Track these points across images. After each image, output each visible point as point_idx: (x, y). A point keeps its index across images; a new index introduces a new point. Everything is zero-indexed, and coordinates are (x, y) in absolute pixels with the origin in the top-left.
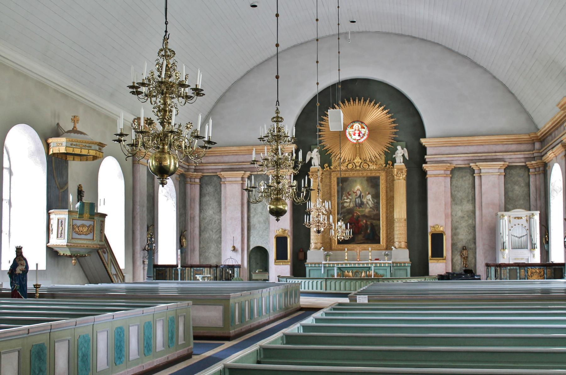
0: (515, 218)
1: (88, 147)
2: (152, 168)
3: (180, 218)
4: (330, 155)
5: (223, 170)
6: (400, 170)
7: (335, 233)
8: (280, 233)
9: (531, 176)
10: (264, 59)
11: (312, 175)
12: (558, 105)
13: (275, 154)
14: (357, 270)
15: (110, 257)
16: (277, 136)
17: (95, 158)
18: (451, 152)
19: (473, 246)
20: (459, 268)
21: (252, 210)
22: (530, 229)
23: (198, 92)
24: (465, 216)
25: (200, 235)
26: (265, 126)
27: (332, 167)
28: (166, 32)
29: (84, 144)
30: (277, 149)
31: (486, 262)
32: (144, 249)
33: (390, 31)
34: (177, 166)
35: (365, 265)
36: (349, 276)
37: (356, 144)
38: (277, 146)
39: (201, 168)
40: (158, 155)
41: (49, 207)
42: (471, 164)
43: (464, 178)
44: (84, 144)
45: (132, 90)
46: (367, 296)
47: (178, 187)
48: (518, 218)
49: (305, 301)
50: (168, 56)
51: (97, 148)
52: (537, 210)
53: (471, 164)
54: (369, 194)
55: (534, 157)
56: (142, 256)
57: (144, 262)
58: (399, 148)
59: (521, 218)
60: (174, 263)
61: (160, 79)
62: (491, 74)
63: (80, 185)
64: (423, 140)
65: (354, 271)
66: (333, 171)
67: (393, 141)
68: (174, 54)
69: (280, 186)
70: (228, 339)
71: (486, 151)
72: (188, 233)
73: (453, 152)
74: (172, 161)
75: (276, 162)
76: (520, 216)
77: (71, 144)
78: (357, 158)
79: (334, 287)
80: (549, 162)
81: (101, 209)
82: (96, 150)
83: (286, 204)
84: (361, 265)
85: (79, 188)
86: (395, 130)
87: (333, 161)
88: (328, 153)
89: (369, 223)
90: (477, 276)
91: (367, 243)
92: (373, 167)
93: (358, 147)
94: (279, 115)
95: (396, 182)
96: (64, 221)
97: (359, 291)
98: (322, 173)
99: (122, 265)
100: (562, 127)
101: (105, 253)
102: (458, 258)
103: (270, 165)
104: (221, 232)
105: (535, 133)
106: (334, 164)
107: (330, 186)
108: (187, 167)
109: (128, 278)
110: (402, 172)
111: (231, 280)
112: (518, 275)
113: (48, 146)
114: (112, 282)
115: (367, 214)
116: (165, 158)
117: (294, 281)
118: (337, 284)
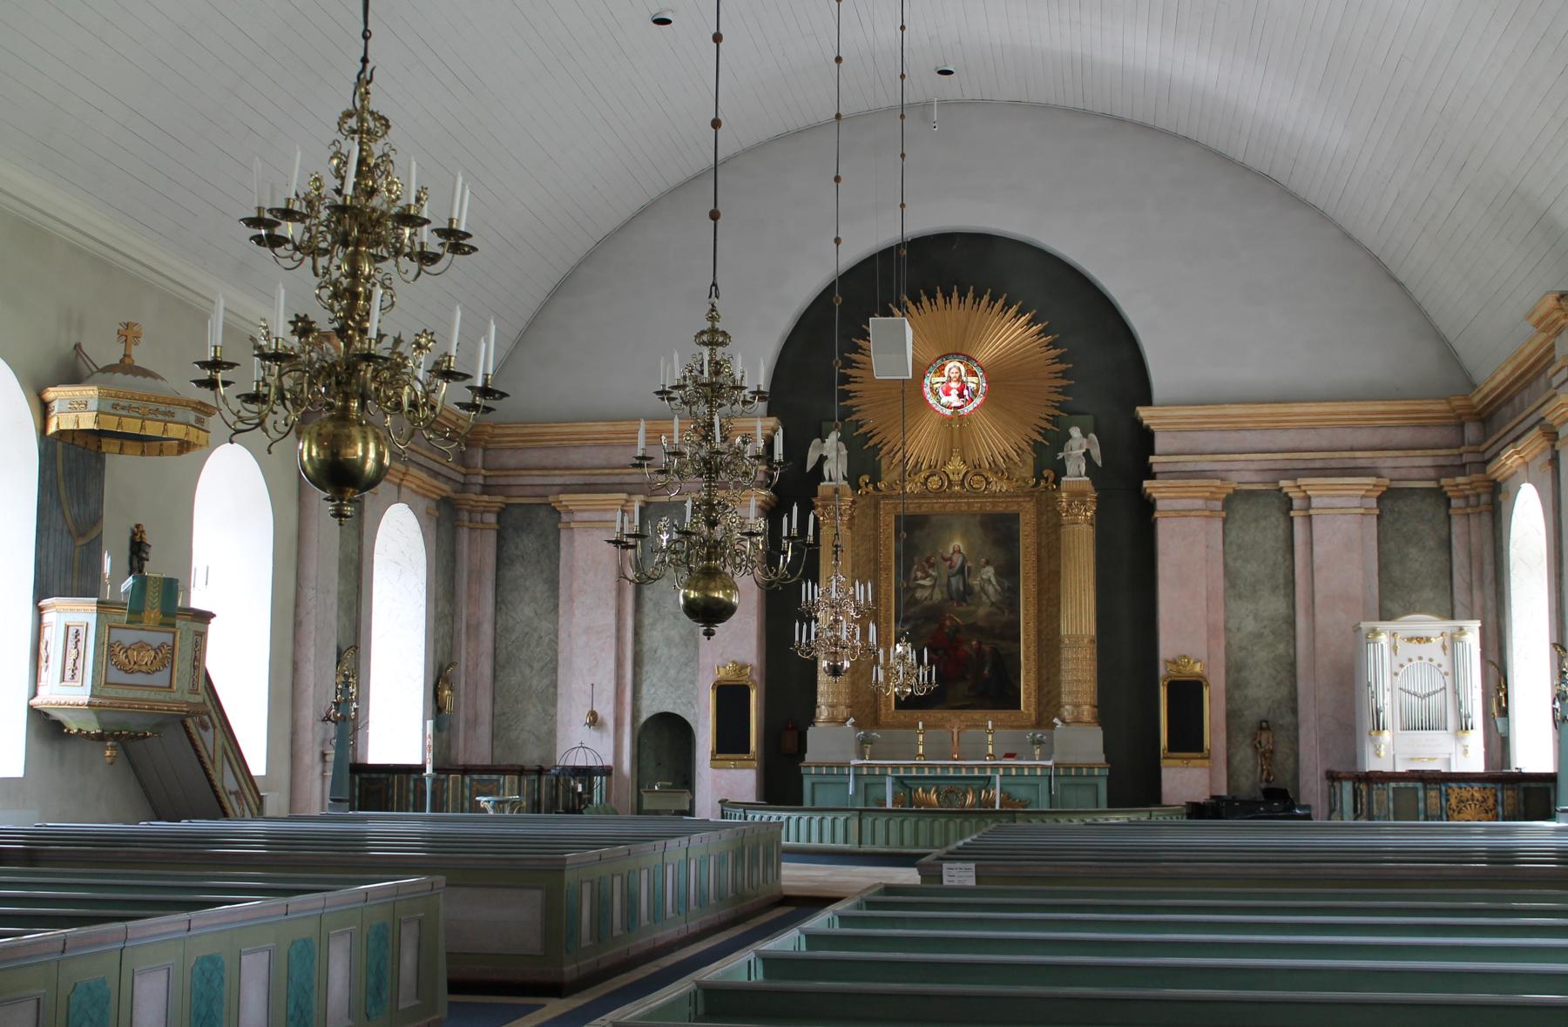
0: (1410, 640)
1: (165, 414)
2: (309, 468)
3: (436, 629)
4: (876, 449)
5: (567, 489)
6: (1078, 495)
7: (887, 678)
8: (726, 673)
9: (1454, 520)
10: (690, 174)
11: (824, 507)
12: (1529, 317)
13: (705, 438)
14: (952, 786)
15: (221, 739)
16: (710, 385)
17: (184, 446)
18: (1226, 447)
19: (1288, 719)
20: (1249, 784)
21: (648, 607)
22: (1454, 672)
23: (455, 240)
24: (1266, 632)
25: (495, 677)
26: (676, 356)
27: (881, 485)
28: (365, 60)
29: (153, 406)
30: (711, 425)
31: (1329, 766)
32: (327, 719)
33: (1053, 102)
34: (386, 461)
35: (976, 773)
36: (931, 805)
37: (950, 419)
38: (711, 414)
39: (502, 481)
40: (330, 427)
41: (43, 590)
42: (1283, 483)
43: (1263, 523)
44: (153, 406)
45: (256, 232)
46: (972, 865)
47: (432, 536)
48: (1419, 640)
49: (796, 876)
50: (369, 132)
51: (192, 417)
52: (1472, 618)
53: (1283, 483)
54: (988, 563)
55: (1463, 466)
56: (318, 740)
57: (324, 755)
58: (1075, 432)
59: (1428, 640)
60: (416, 760)
61: (339, 201)
62: (1339, 227)
63: (138, 526)
64: (1143, 412)
65: (944, 788)
66: (886, 497)
67: (1057, 412)
68: (388, 127)
69: (718, 533)
70: (556, 990)
71: (1324, 443)
72: (460, 673)
73: (1230, 447)
74: (372, 446)
75: (706, 462)
76: (1423, 634)
77: (115, 406)
78: (962, 469)
79: (880, 837)
80: (1506, 480)
81: (198, 599)
82: (188, 424)
83: (734, 587)
84: (964, 773)
85: (134, 534)
86: (1065, 382)
87: (884, 466)
88: (871, 443)
89: (986, 648)
90: (1302, 807)
91: (982, 707)
92: (1000, 486)
93: (956, 426)
94: (717, 325)
95: (1066, 531)
96: (82, 631)
97: (952, 847)
98: (853, 502)
99: (257, 765)
100: (1542, 380)
101: (205, 728)
102: (1245, 753)
103: (689, 470)
104: (555, 670)
105: (1466, 397)
106: (889, 477)
107: (876, 539)
108: (461, 479)
109: (275, 802)
110: (1084, 503)
111: (581, 812)
112: (1421, 805)
113: (44, 410)
114: (225, 815)
115: (980, 623)
116: (349, 437)
117: (766, 815)
118: (894, 825)
